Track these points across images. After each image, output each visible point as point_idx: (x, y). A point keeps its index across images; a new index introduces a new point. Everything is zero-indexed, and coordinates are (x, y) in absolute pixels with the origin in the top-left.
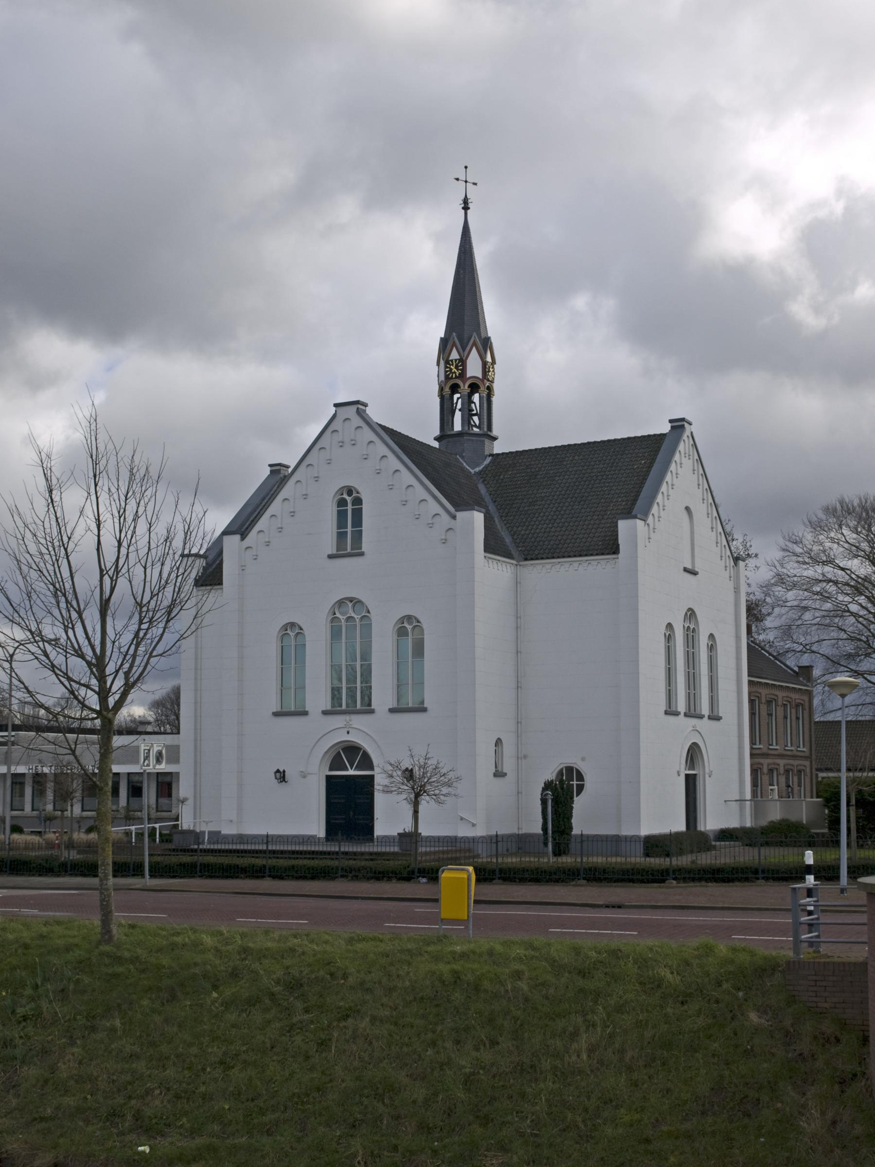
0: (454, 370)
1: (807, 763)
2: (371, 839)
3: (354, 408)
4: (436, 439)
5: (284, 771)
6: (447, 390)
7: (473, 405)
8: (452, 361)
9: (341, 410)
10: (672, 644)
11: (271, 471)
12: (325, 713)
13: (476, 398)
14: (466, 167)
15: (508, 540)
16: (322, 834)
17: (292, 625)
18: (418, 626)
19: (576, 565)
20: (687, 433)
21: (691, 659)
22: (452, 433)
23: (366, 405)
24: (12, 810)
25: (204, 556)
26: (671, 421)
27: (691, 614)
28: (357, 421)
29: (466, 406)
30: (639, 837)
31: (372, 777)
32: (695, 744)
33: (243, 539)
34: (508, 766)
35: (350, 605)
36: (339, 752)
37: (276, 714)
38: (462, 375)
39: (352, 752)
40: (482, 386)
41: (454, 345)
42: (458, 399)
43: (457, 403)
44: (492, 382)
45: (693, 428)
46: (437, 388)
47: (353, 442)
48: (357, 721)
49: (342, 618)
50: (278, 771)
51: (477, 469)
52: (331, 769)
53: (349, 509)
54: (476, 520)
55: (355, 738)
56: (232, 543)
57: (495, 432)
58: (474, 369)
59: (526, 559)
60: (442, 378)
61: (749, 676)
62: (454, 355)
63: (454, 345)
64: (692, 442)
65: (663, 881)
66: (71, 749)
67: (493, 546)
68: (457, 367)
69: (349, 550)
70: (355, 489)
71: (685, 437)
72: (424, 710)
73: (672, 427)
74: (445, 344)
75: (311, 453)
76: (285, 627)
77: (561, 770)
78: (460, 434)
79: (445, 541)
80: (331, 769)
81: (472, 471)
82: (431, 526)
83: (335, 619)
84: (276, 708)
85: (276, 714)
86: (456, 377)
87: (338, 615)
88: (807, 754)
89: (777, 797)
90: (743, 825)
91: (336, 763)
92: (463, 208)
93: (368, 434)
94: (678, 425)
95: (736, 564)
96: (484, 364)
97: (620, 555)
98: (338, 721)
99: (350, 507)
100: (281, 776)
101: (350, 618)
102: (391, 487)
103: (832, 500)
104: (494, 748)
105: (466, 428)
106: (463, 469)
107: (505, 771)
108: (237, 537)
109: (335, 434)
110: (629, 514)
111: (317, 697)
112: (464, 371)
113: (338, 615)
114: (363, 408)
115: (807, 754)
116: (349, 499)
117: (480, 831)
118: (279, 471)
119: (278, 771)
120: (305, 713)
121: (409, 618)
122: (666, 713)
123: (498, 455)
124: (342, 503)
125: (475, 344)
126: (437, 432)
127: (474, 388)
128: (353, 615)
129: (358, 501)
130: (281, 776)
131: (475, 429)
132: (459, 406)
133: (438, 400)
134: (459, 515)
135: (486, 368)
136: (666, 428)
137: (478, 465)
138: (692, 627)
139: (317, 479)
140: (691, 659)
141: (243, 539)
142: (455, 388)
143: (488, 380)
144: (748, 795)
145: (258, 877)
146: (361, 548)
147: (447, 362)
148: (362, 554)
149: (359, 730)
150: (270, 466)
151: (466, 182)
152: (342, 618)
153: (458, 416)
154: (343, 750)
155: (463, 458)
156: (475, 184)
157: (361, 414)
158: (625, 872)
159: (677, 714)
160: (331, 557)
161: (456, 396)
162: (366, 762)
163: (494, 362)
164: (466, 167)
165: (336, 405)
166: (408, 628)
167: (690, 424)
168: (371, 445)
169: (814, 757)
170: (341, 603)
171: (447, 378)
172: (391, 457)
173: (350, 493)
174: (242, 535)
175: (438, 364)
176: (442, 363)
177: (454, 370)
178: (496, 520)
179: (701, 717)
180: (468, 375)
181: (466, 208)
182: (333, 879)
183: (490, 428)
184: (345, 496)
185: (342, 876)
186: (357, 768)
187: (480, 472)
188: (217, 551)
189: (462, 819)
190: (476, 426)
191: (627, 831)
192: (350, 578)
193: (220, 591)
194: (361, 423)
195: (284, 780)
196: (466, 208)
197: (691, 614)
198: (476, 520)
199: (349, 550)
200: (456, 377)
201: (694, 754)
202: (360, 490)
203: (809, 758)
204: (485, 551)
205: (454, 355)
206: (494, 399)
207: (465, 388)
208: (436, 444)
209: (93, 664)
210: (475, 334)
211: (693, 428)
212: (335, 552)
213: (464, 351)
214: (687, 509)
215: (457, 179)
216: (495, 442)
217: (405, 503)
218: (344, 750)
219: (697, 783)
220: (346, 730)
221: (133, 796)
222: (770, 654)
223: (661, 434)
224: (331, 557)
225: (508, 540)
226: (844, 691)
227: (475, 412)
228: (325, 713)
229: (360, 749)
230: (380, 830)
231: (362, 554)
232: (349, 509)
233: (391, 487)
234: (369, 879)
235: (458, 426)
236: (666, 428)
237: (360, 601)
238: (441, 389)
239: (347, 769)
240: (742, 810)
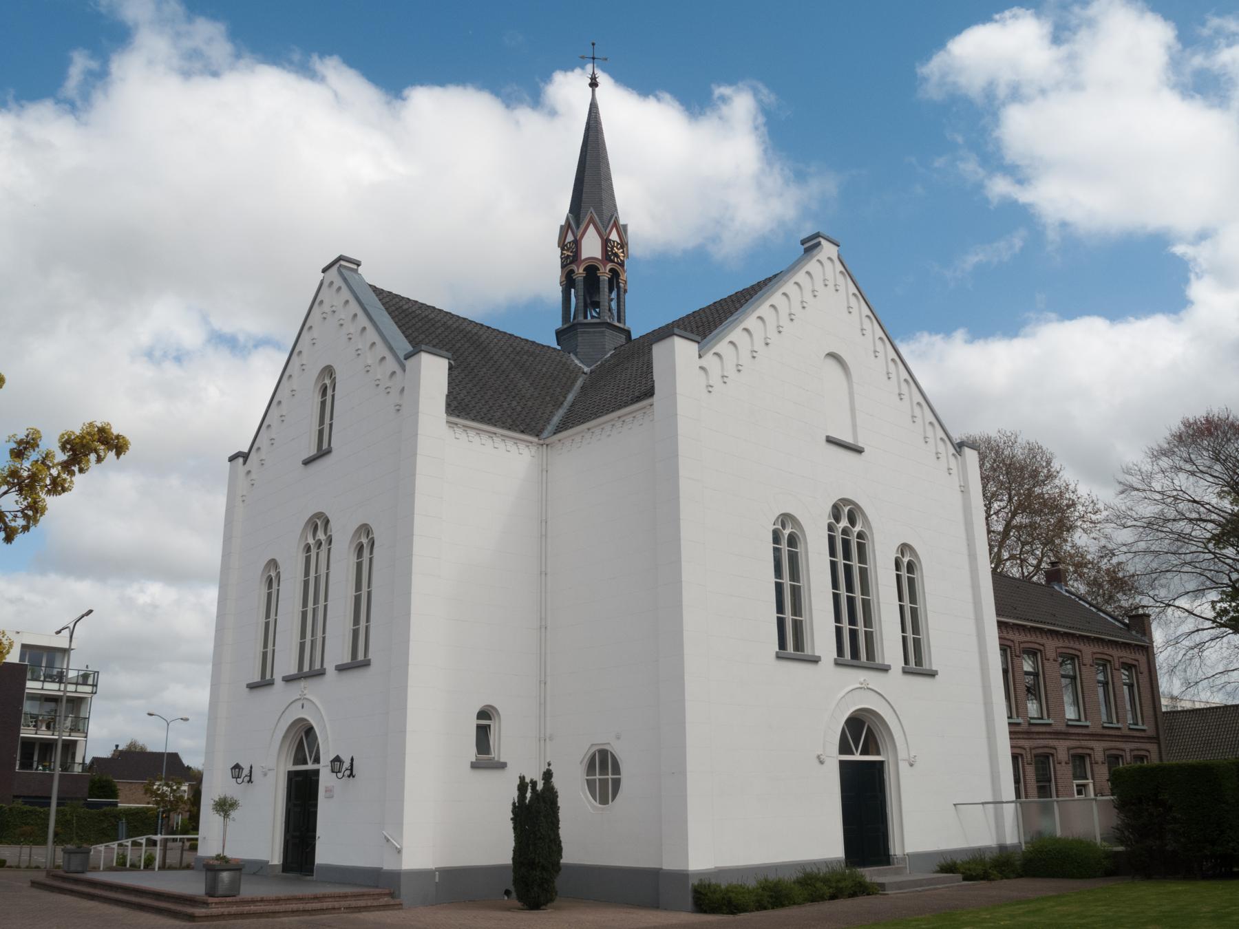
16: (276, 859)
30: (683, 876)
52: (295, 763)
61: (998, 614)
62: (570, 238)
74: (565, 230)
80: (295, 763)
89: (1092, 796)
90: (1002, 842)
95: (959, 453)
103: (1176, 425)
107: (502, 760)
125: (592, 221)
144: (1009, 792)
169: (1161, 737)
203: (1155, 739)
208: (554, 344)
213: (578, 227)
219: (886, 777)
222: (1091, 605)
240: (999, 818)
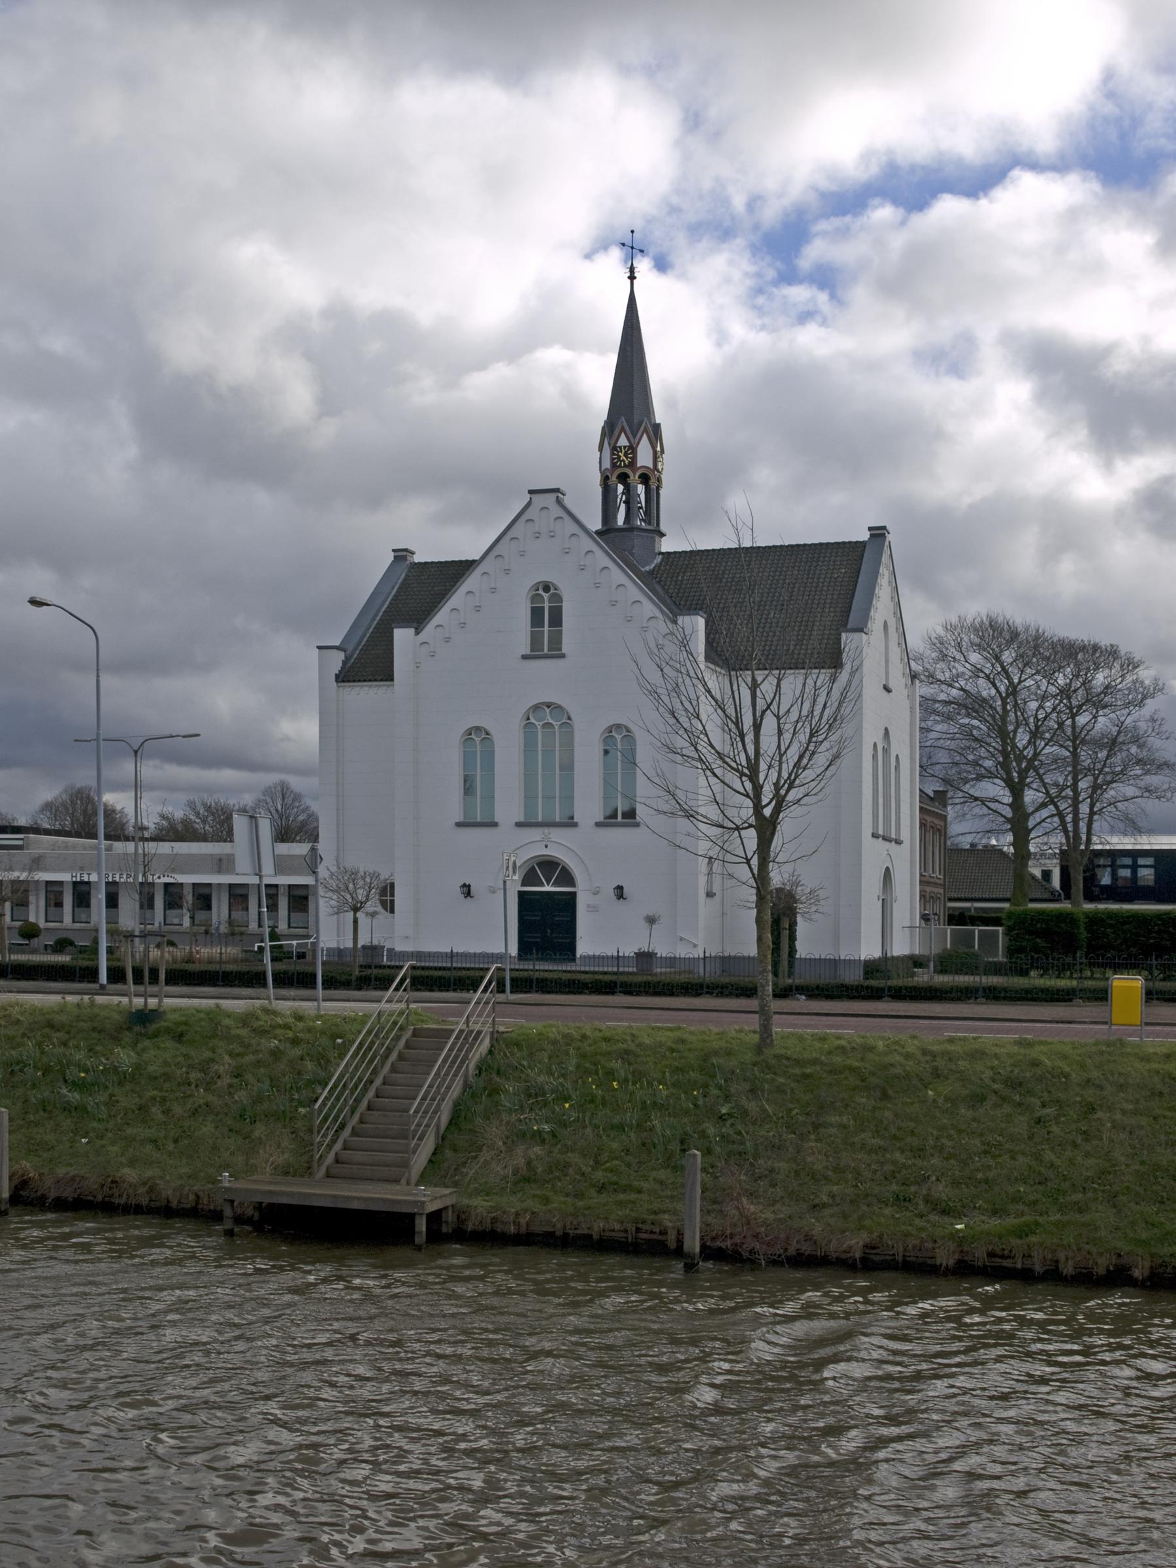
0: (623, 458)
1: (942, 891)
2: (574, 960)
3: (553, 496)
9: (535, 497)
14: (632, 232)
16: (514, 950)
17: (478, 729)
18: (629, 736)
24: (47, 921)
26: (870, 529)
28: (556, 511)
31: (574, 894)
33: (417, 633)
34: (716, 888)
35: (548, 710)
37: (459, 825)
38: (632, 464)
39: (549, 866)
46: (597, 477)
49: (539, 724)
52: (523, 884)
55: (553, 852)
58: (644, 457)
60: (607, 464)
62: (623, 441)
63: (623, 430)
65: (1070, 1000)
66: (746, 858)
67: (714, 653)
68: (626, 455)
69: (546, 651)
70: (553, 584)
72: (575, 825)
73: (871, 535)
74: (610, 429)
75: (501, 542)
76: (469, 732)
80: (523, 884)
83: (528, 725)
84: (460, 818)
85: (459, 825)
86: (625, 466)
87: (532, 720)
88: (941, 882)
91: (530, 877)
94: (878, 534)
96: (655, 452)
98: (535, 834)
100: (467, 890)
101: (548, 725)
102: (597, 586)
109: (530, 524)
111: (508, 805)
112: (634, 459)
113: (532, 720)
115: (941, 882)
117: (698, 953)
118: (404, 558)
120: (494, 825)
124: (535, 598)
128: (551, 721)
129: (557, 598)
130: (467, 890)
133: (599, 490)
136: (864, 536)
137: (647, 564)
139: (507, 571)
141: (417, 633)
145: (607, 993)
146: (560, 649)
147: (614, 449)
148: (563, 656)
149: (558, 845)
150: (394, 551)
152: (539, 724)
157: (559, 502)
158: (1027, 991)
160: (525, 657)
162: (566, 877)
163: (662, 451)
165: (531, 492)
168: (574, 538)
170: (536, 708)
171: (614, 466)
172: (599, 553)
173: (547, 588)
175: (601, 448)
177: (623, 458)
180: (639, 465)
182: (613, 993)
184: (541, 592)
185: (707, 993)
186: (555, 884)
189: (681, 939)
191: (844, 954)
192: (546, 681)
194: (560, 512)
199: (546, 651)
200: (625, 466)
202: (560, 585)
205: (623, 441)
206: (661, 492)
209: (746, 775)
212: (528, 652)
213: (634, 437)
218: (540, 864)
220: (543, 844)
221: (79, 906)
224: (525, 657)
229: (557, 864)
230: (583, 948)
231: (563, 656)
234: (737, 996)
236: (864, 536)
237: (559, 707)
239: (542, 885)
240: (912, 936)
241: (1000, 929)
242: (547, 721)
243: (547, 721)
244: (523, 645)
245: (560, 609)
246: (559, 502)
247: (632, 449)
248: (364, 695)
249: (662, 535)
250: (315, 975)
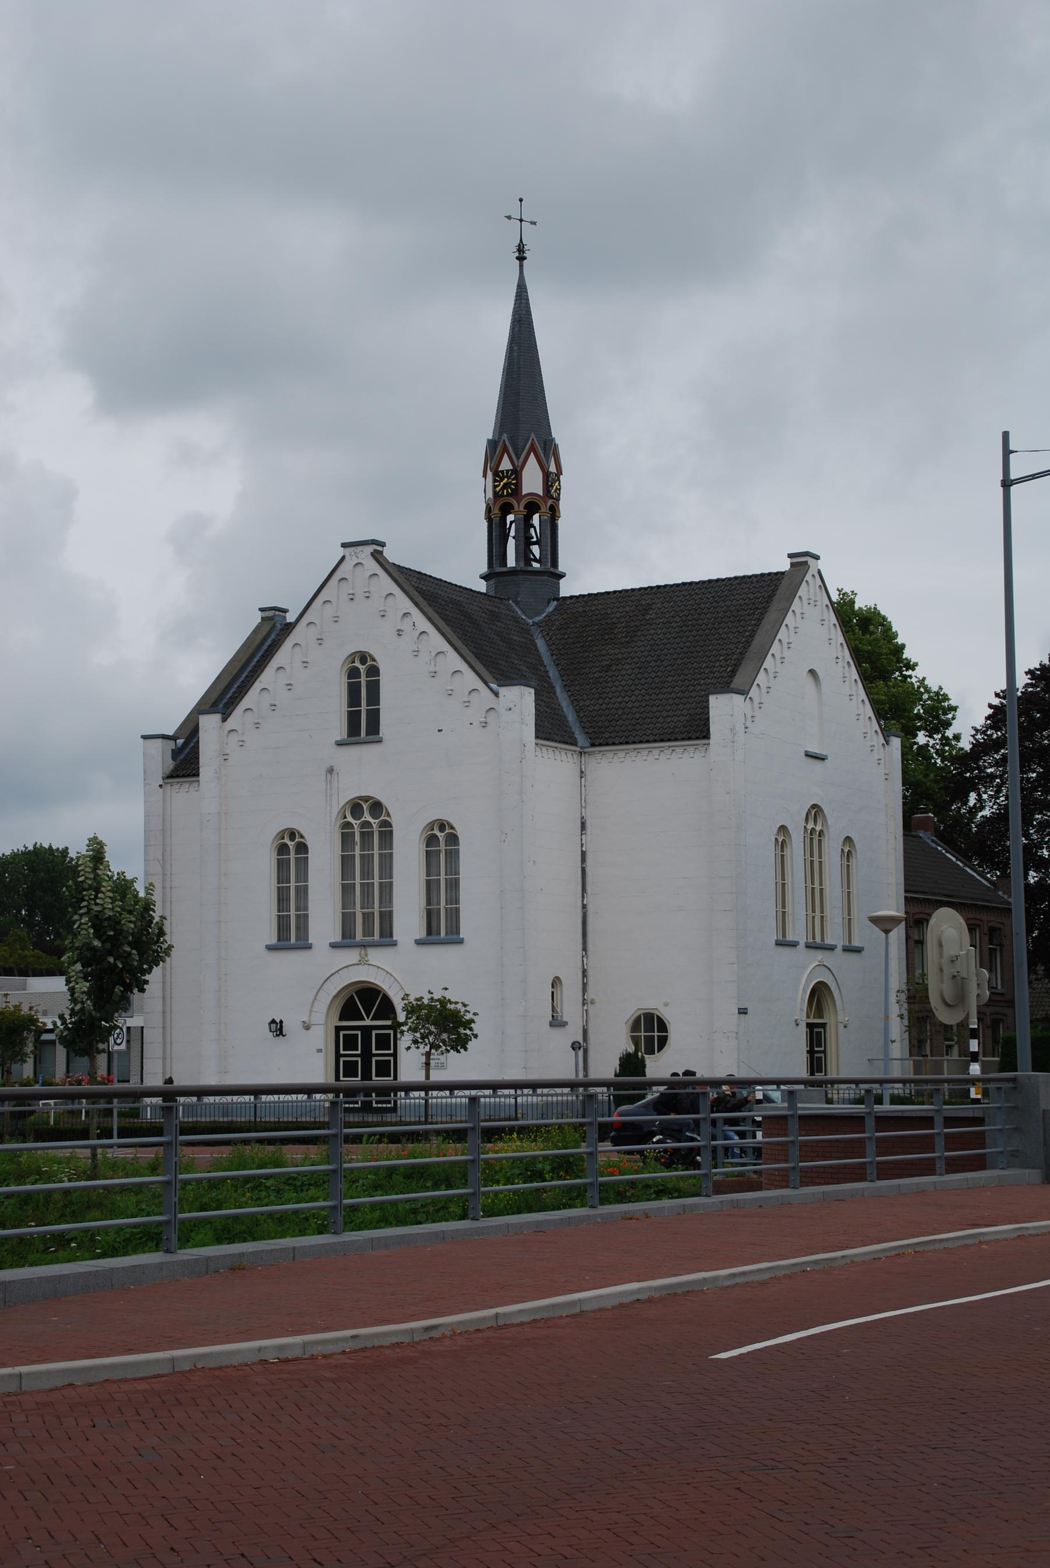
4: (485, 577)
5: (281, 1022)
6: (496, 510)
7: (532, 531)
8: (502, 472)
10: (787, 852)
11: (262, 618)
12: (334, 946)
13: (536, 519)
14: (521, 200)
15: (571, 717)
19: (656, 752)
20: (812, 571)
21: (814, 869)
22: (504, 569)
23: (383, 545)
25: (173, 738)
27: (816, 812)
28: (372, 566)
29: (522, 534)
32: (821, 984)
36: (352, 996)
38: (516, 491)
40: (548, 504)
41: (505, 450)
42: (511, 523)
43: (510, 528)
44: (558, 499)
45: (821, 565)
47: (367, 594)
48: (378, 956)
50: (273, 1021)
51: (537, 619)
52: (341, 1019)
53: (363, 685)
54: (521, 701)
56: (209, 723)
57: (561, 568)
58: (532, 482)
59: (593, 745)
62: (506, 465)
63: (505, 450)
64: (819, 582)
71: (808, 577)
73: (792, 565)
74: (494, 450)
77: (639, 1017)
78: (513, 572)
79: (485, 725)
80: (341, 1019)
81: (530, 621)
82: (467, 704)
91: (348, 1011)
92: (517, 258)
93: (384, 579)
94: (801, 562)
96: (546, 475)
97: (711, 741)
98: (351, 956)
99: (363, 679)
100: (278, 1028)
101: (367, 824)
104: (550, 990)
105: (522, 564)
106: (517, 620)
108: (217, 718)
109: (343, 583)
110: (725, 687)
114: (380, 548)
116: (362, 668)
119: (273, 1021)
121: (442, 825)
122: (779, 944)
123: (565, 598)
125: (533, 449)
126: (484, 569)
127: (532, 507)
129: (374, 671)
130: (278, 1028)
131: (536, 565)
132: (512, 533)
134: (503, 691)
135: (551, 481)
136: (784, 565)
137: (539, 614)
138: (818, 828)
140: (814, 869)
141: (224, 720)
142: (506, 509)
143: (552, 498)
147: (496, 473)
151: (521, 220)
153: (511, 544)
154: (356, 993)
155: (517, 603)
156: (534, 223)
157: (377, 556)
159: (794, 945)
161: (510, 518)
163: (559, 472)
164: (521, 200)
165: (344, 545)
166: (442, 842)
167: (817, 558)
168: (390, 598)
173: (363, 661)
174: (223, 714)
175: (485, 475)
176: (490, 474)
178: (558, 690)
179: (831, 948)
181: (521, 259)
183: (555, 562)
187: (541, 622)
188: (192, 726)
190: (536, 560)
192: (365, 772)
193: (196, 785)
195: (281, 1033)
196: (521, 259)
197: (816, 812)
198: (521, 701)
201: (819, 996)
204: (537, 737)
205: (506, 465)
206: (561, 523)
207: (520, 507)
208: (481, 587)
210: (533, 436)
211: (821, 565)
213: (518, 458)
214: (812, 672)
215: (509, 218)
216: (561, 581)
217: (434, 674)
218: (358, 993)
223: (777, 573)
225: (571, 717)
226: (887, 926)
227: (535, 539)
228: (334, 946)
232: (363, 685)
233: (416, 653)
235: (511, 562)
238: (489, 510)
241: (359, 1078)
242: (366, 824)
243: (366, 824)
244: (339, 729)
245: (377, 683)
246: (377, 556)
247: (517, 473)
248: (181, 794)
249: (562, 576)
250: (112, 1129)
